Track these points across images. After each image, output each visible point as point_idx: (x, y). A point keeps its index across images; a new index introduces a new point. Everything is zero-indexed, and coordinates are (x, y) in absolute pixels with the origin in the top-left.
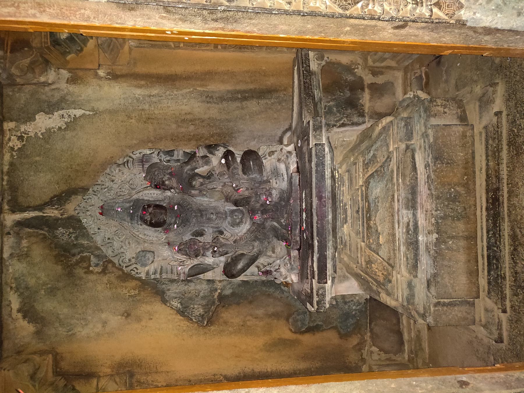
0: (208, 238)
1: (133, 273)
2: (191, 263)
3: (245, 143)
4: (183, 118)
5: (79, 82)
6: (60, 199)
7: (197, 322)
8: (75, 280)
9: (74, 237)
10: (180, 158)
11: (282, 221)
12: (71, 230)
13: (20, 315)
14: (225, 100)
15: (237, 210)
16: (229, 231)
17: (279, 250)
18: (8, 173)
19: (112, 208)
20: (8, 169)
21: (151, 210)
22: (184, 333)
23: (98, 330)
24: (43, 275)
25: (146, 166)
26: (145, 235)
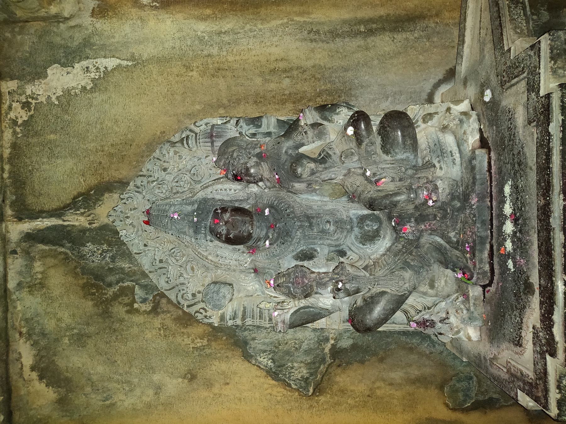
1: (200, 317)
2: (293, 306)
3: (372, 105)
4: (272, 67)
5: (110, 14)
6: (87, 199)
7: (297, 390)
8: (113, 322)
9: (109, 257)
10: (272, 129)
11: (452, 234)
12: (105, 247)
13: (34, 375)
14: (338, 35)
15: (370, 215)
16: (356, 251)
17: (443, 283)
18: (11, 160)
19: (163, 213)
20: (10, 154)
21: (227, 216)
22: (277, 406)
23: (149, 399)
24: (66, 315)
25: (218, 143)
26: (217, 256)
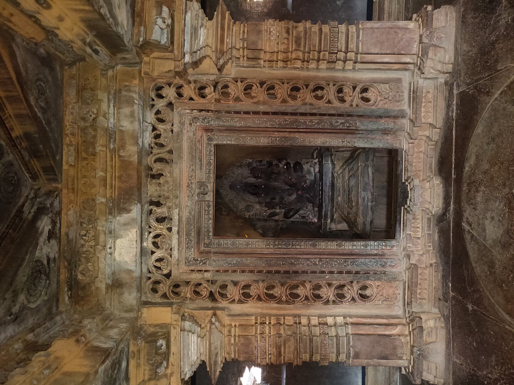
0: (277, 201)
25: (250, 168)
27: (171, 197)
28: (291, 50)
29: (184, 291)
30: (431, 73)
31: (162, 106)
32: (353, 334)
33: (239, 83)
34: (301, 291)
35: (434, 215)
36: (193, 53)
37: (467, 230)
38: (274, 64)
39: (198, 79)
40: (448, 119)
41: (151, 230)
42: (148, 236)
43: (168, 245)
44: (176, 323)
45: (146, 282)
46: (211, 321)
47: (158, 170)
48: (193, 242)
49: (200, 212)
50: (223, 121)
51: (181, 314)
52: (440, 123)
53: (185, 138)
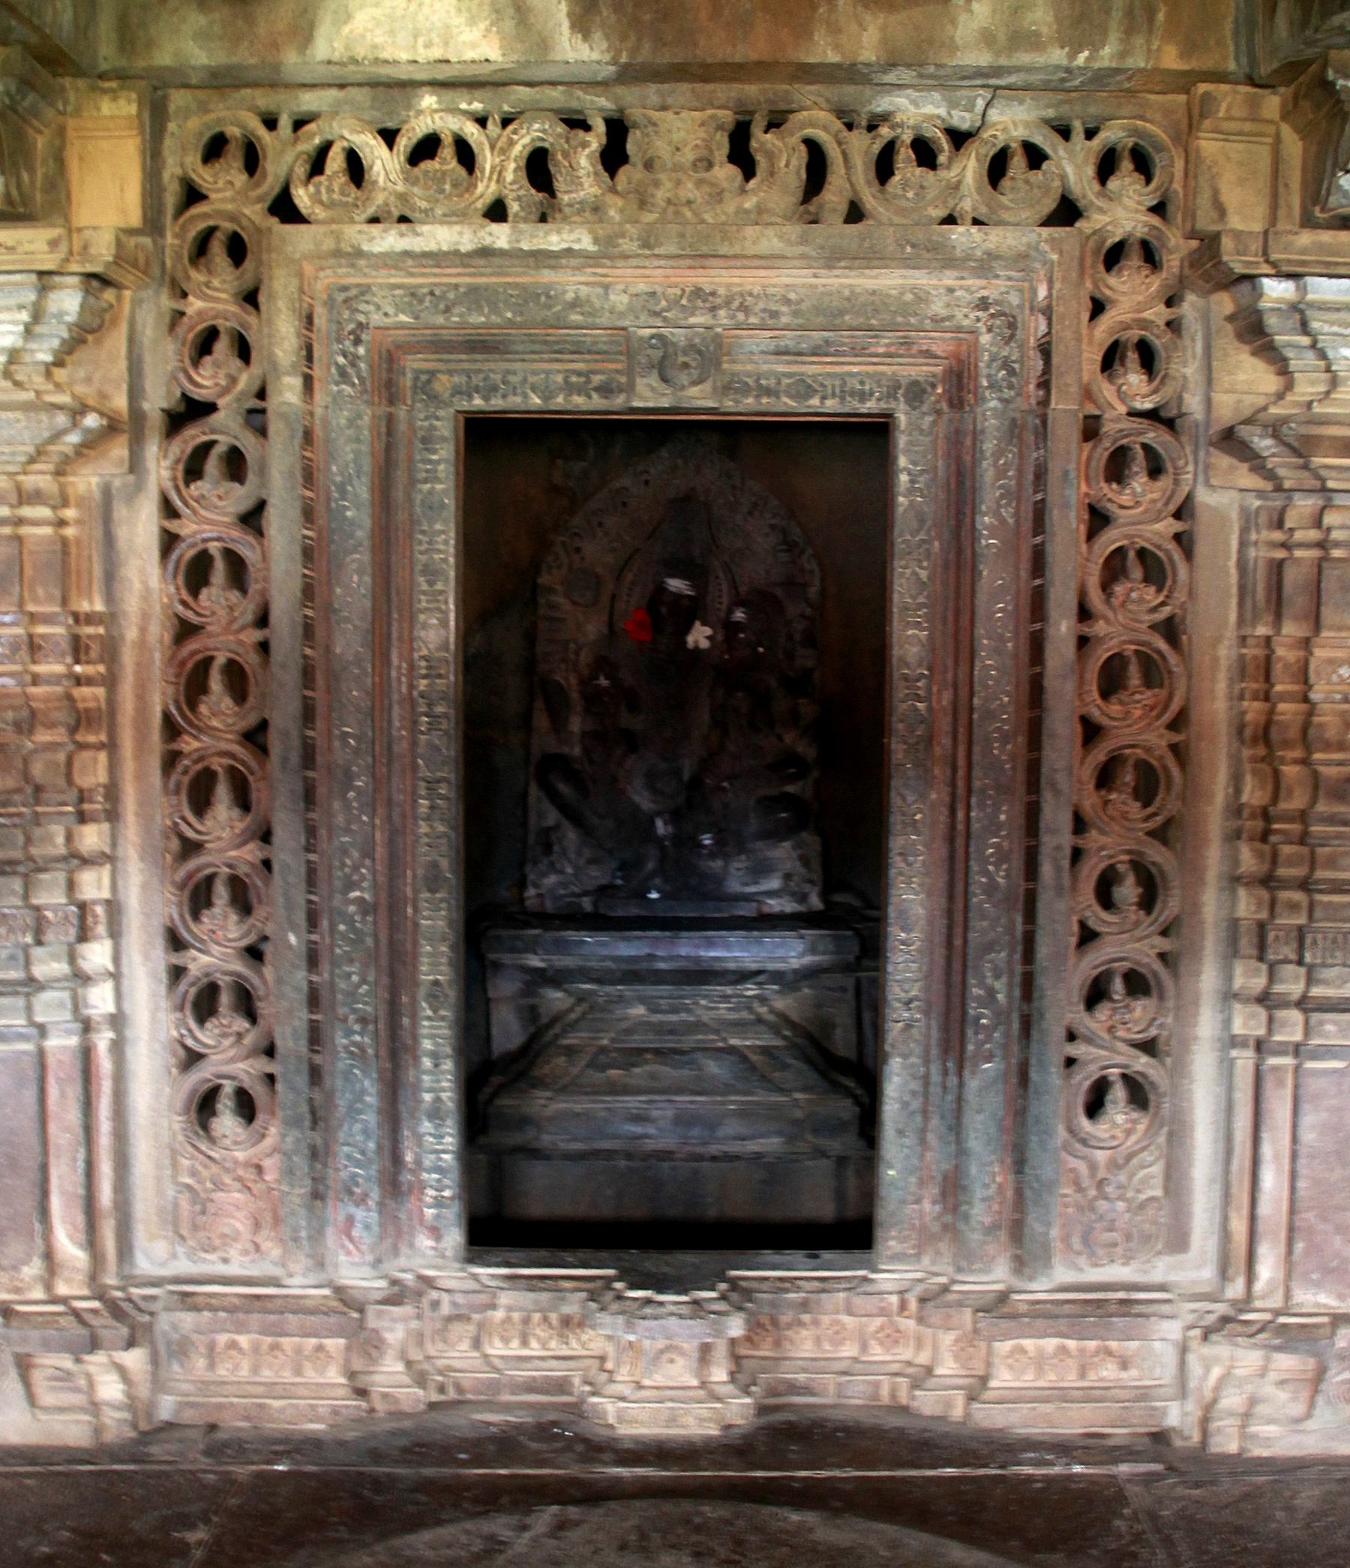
25: (779, 592)
27: (650, 217)
28: (1317, 756)
29: (216, 283)
30: (1207, 1370)
31: (1063, 177)
32: (41, 1054)
33: (1173, 526)
34: (223, 820)
35: (583, 1402)
36: (1300, 313)
37: (528, 1521)
38: (1254, 686)
39: (1187, 342)
40: (1004, 1447)
41: (493, 128)
42: (465, 113)
43: (424, 205)
44: (76, 248)
45: (253, 109)
46: (78, 411)
47: (771, 156)
48: (440, 320)
49: (578, 349)
50: (999, 453)
51: (114, 275)
52: (991, 1417)
53: (921, 279)
